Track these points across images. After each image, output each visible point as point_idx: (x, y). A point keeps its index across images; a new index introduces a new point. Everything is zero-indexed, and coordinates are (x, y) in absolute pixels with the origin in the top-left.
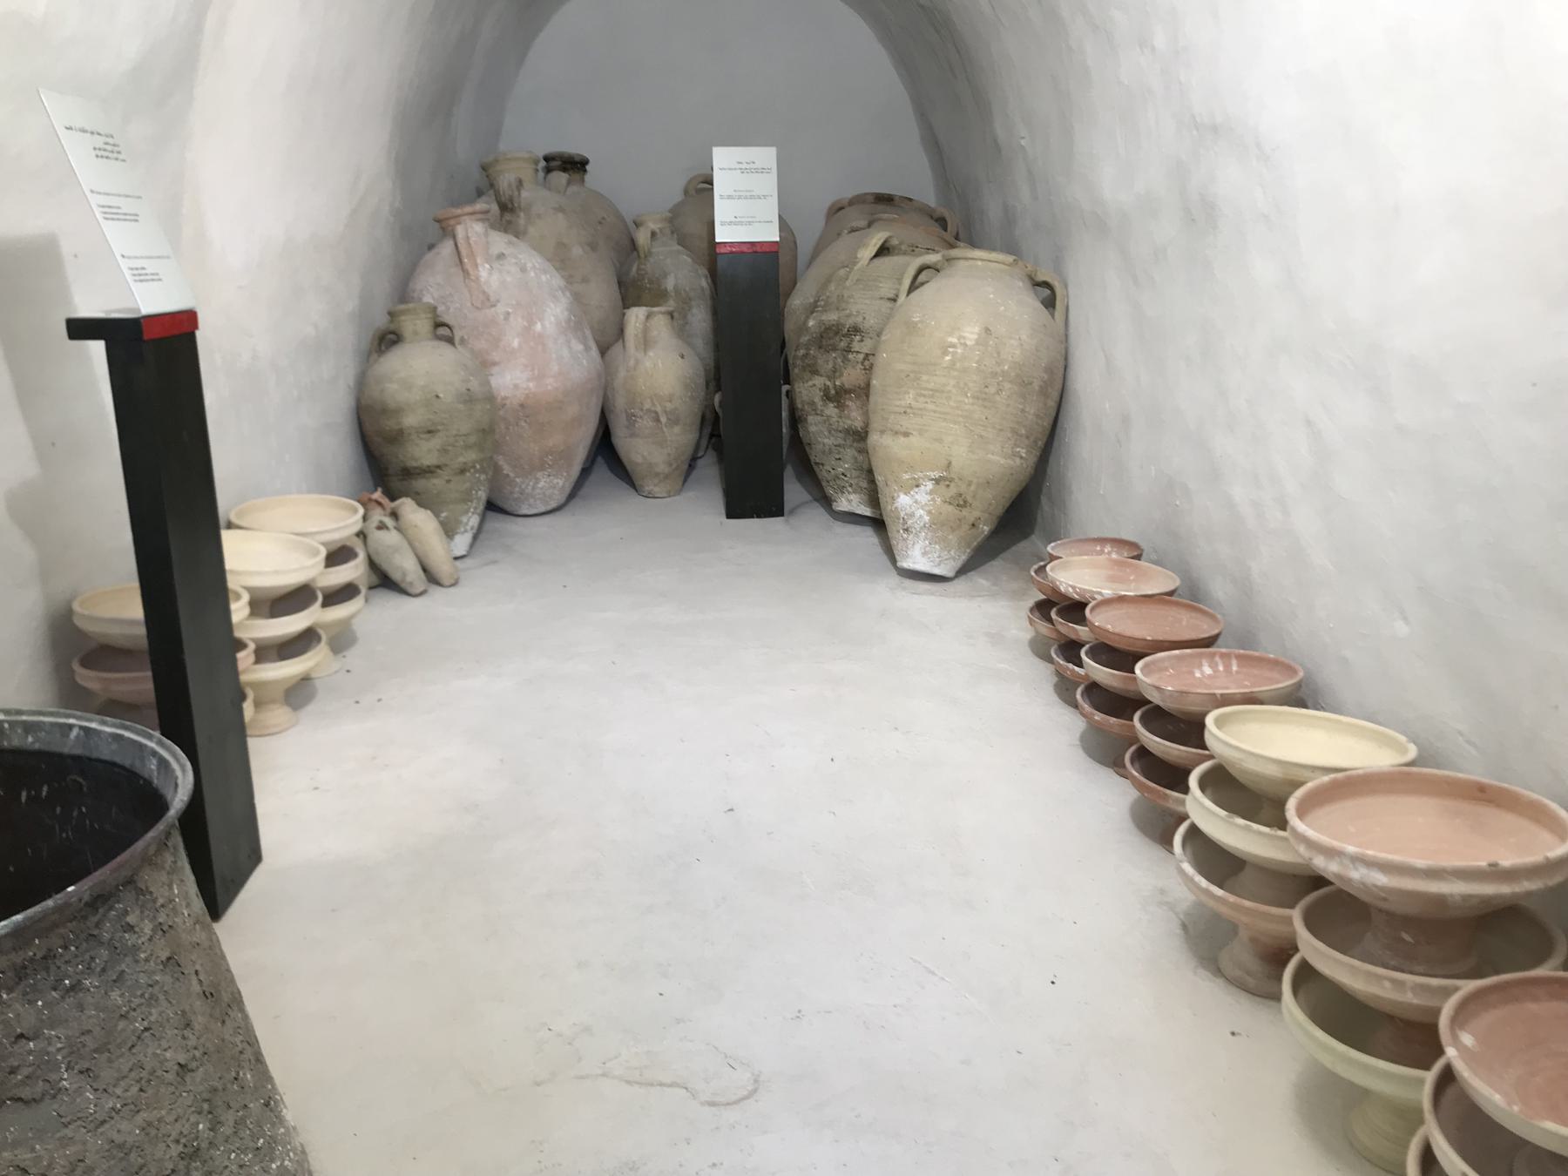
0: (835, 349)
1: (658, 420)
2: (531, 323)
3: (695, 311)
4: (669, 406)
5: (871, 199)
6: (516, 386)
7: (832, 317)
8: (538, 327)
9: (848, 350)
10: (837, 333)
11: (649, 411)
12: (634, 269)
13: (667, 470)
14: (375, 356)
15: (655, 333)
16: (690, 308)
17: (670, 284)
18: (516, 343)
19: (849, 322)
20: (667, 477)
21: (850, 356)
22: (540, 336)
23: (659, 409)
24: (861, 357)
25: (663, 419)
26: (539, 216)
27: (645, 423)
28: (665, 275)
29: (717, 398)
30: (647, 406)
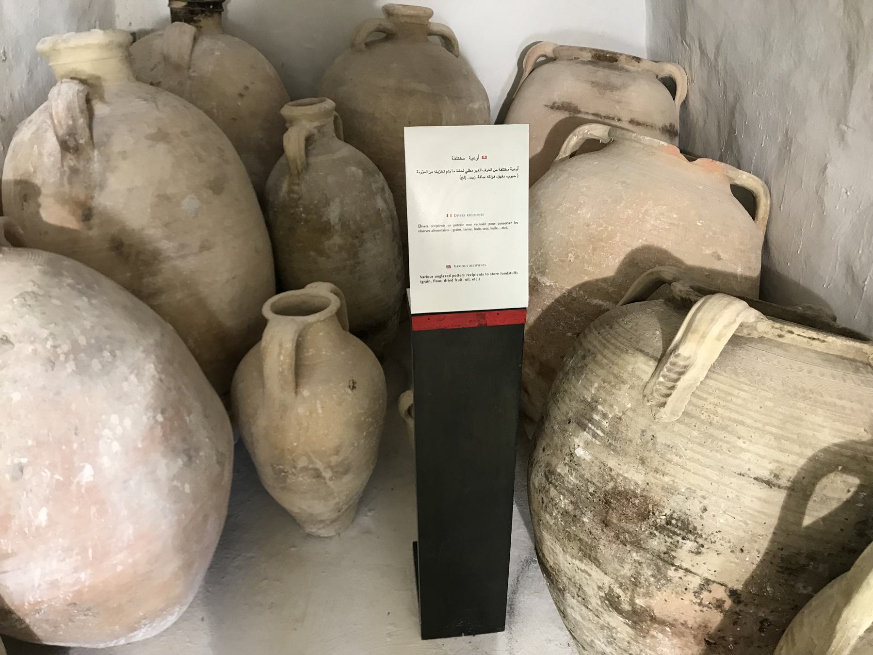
0: (638, 545)
1: (318, 475)
2: (70, 470)
3: (369, 245)
4: (334, 460)
5: (587, 56)
6: (54, 584)
7: (632, 475)
8: (87, 474)
9: (666, 559)
10: (644, 516)
11: (305, 469)
12: (285, 187)
13: (334, 516)
14: (25, 204)
15: (311, 352)
16: (362, 242)
17: (333, 213)
18: (42, 517)
19: (671, 506)
20: (333, 521)
21: (671, 572)
22: (92, 489)
23: (319, 465)
24: (695, 582)
25: (327, 474)
26: (124, 155)
27: (304, 480)
28: (327, 204)
29: (407, 399)
30: (302, 462)
